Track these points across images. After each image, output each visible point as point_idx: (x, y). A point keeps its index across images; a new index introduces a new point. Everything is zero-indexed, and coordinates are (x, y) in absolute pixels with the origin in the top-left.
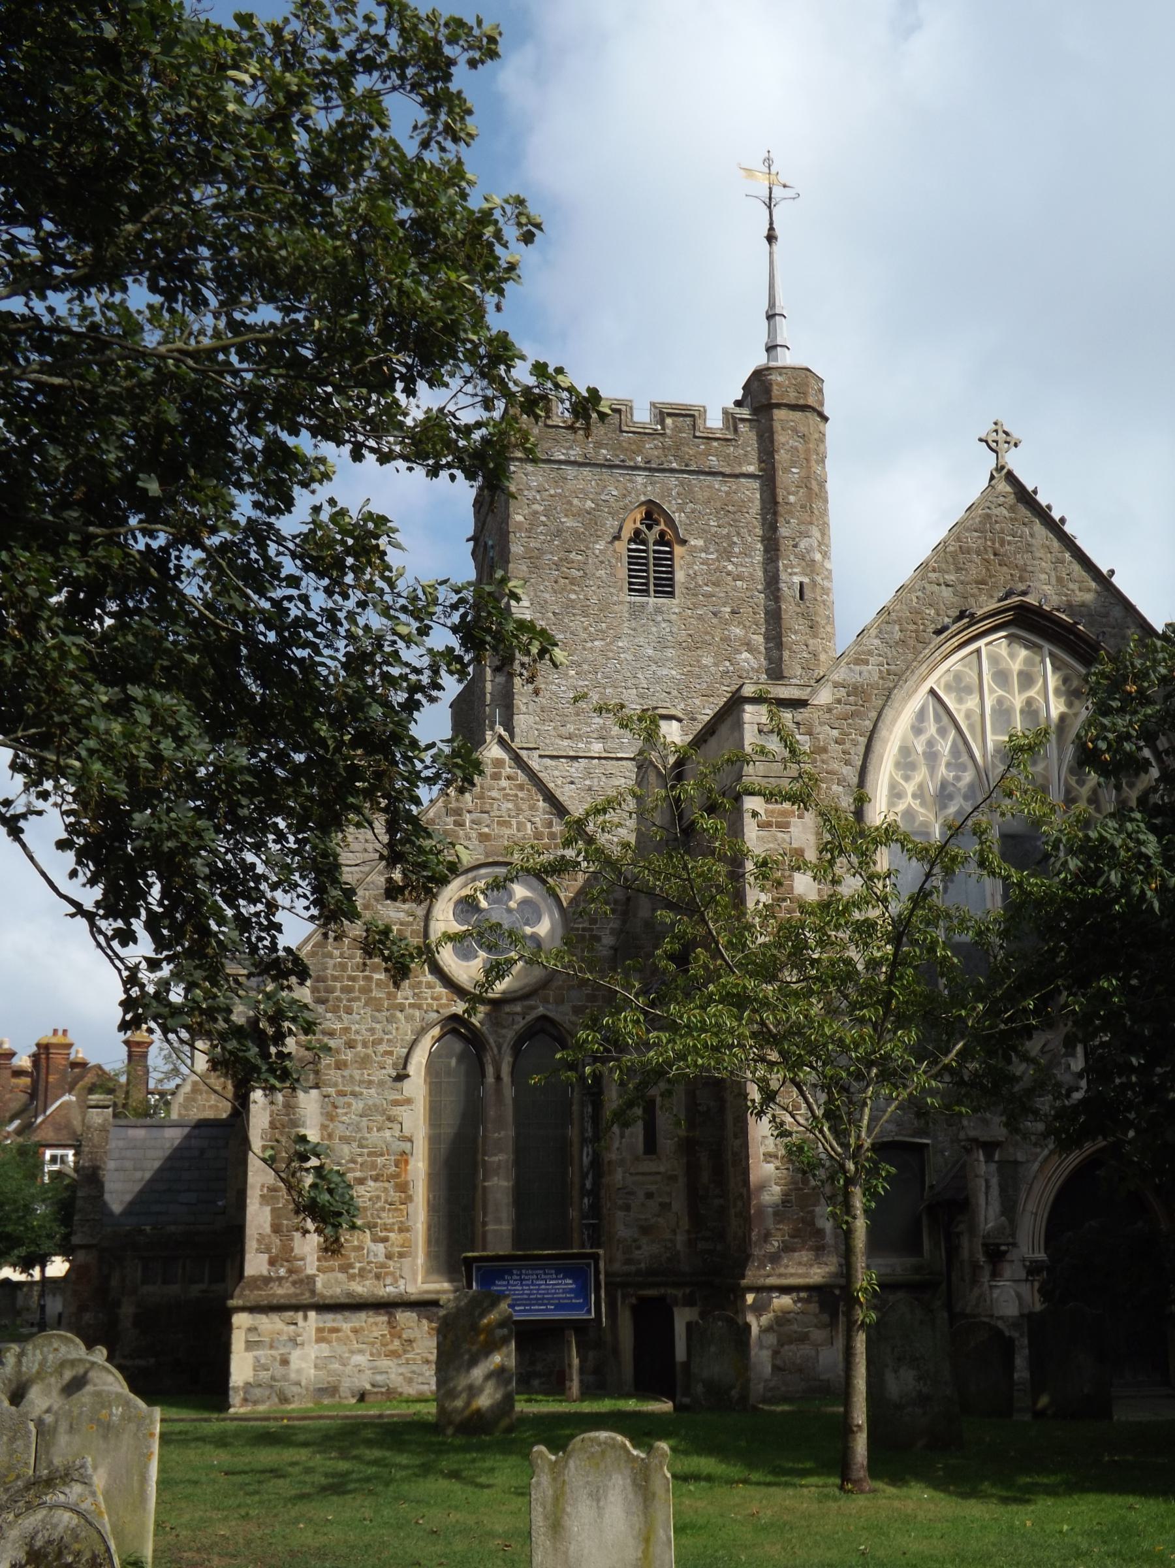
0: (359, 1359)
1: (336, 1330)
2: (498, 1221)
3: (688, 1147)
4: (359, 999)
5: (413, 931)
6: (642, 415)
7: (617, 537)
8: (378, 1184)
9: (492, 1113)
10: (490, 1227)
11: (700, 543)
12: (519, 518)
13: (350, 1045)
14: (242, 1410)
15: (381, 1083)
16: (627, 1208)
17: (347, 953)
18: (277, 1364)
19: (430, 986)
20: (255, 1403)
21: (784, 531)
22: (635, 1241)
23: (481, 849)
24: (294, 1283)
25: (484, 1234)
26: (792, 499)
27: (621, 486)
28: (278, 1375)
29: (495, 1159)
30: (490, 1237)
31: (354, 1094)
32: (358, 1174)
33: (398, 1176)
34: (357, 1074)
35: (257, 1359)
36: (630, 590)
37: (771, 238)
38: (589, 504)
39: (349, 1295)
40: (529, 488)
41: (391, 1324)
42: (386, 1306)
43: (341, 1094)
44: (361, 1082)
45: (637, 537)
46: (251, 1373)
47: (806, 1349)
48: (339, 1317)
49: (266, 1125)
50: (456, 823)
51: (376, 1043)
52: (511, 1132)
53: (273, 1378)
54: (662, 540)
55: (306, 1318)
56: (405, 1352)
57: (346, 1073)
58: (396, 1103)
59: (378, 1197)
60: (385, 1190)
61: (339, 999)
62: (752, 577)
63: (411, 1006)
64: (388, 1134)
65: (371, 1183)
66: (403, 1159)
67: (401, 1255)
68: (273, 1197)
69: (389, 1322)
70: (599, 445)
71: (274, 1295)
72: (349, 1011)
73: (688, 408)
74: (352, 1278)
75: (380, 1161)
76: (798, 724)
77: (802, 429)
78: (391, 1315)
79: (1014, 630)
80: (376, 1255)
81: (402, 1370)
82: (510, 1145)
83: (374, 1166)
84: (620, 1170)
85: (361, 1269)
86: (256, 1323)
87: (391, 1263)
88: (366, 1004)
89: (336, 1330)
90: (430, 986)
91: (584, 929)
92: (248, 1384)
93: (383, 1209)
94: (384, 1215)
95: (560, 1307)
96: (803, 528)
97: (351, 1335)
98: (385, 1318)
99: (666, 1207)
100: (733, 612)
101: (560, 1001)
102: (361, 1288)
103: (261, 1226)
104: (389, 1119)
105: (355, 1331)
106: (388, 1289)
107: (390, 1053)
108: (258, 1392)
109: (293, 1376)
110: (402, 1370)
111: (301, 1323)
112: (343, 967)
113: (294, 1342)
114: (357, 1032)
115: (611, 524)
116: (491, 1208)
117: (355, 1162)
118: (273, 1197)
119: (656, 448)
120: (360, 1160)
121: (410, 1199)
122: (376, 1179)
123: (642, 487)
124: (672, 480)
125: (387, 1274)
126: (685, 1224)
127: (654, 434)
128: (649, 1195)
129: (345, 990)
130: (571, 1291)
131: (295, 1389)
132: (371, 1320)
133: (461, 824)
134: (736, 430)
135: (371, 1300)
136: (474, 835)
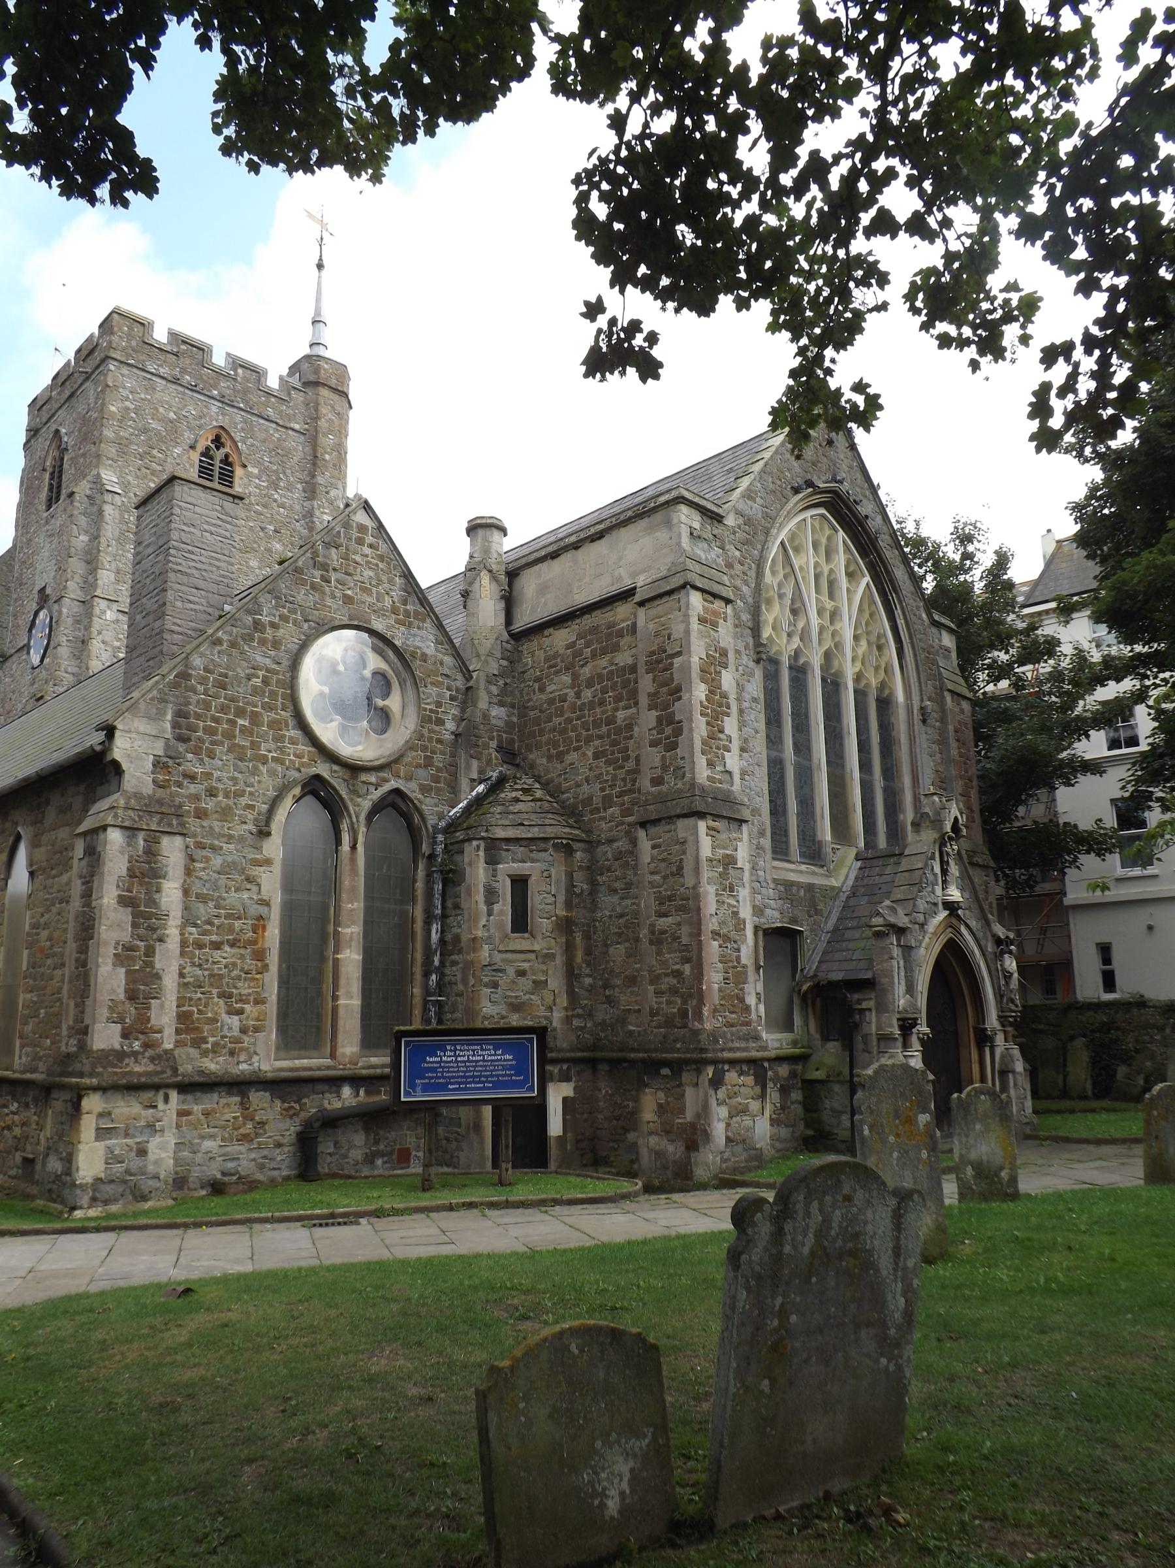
0: (208, 1144)
2: (349, 996)
3: (565, 926)
4: (222, 744)
5: (278, 681)
6: (219, 359)
8: (233, 951)
9: (346, 882)
10: (341, 1002)
11: (256, 471)
12: (113, 409)
13: (212, 793)
14: (92, 1213)
15: (241, 839)
16: (495, 985)
17: (212, 691)
18: (133, 1154)
19: (293, 742)
20: (106, 1202)
21: (320, 479)
25: (335, 1010)
26: (327, 457)
28: (134, 1169)
29: (348, 930)
31: (213, 848)
32: (214, 938)
33: (255, 942)
34: (216, 824)
35: (110, 1149)
37: (320, 266)
38: (172, 415)
39: (201, 1073)
40: (124, 388)
41: (244, 1106)
42: (239, 1086)
43: (202, 846)
45: (206, 453)
49: (124, 873)
53: (128, 1172)
54: (226, 460)
55: (166, 1099)
56: (257, 1135)
57: (205, 823)
59: (234, 965)
60: (242, 957)
64: (246, 895)
65: (227, 948)
66: (260, 924)
67: (257, 1029)
68: (129, 958)
69: (242, 1103)
70: (184, 371)
71: (131, 1073)
72: (211, 756)
73: (255, 366)
74: (205, 1053)
75: (237, 924)
78: (244, 1095)
79: (822, 511)
80: (230, 1029)
81: (253, 1155)
82: (361, 917)
83: (231, 929)
84: (486, 947)
85: (215, 1044)
86: (109, 1106)
87: (246, 1038)
88: (229, 751)
90: (293, 742)
91: (431, 711)
92: (98, 1180)
93: (239, 978)
94: (240, 984)
95: (498, 1085)
98: (238, 1099)
100: (276, 531)
101: (409, 778)
102: (212, 1065)
103: (114, 991)
104: (249, 880)
105: (206, 1114)
107: (252, 807)
108: (109, 1189)
109: (151, 1168)
110: (253, 1155)
111: (161, 1106)
112: (207, 706)
115: (188, 436)
118: (129, 958)
121: (266, 967)
122: (232, 945)
125: (241, 1049)
126: (563, 1001)
128: (521, 973)
130: (511, 1068)
131: (153, 1183)
132: (223, 1101)
135: (227, 1078)
136: (338, 594)
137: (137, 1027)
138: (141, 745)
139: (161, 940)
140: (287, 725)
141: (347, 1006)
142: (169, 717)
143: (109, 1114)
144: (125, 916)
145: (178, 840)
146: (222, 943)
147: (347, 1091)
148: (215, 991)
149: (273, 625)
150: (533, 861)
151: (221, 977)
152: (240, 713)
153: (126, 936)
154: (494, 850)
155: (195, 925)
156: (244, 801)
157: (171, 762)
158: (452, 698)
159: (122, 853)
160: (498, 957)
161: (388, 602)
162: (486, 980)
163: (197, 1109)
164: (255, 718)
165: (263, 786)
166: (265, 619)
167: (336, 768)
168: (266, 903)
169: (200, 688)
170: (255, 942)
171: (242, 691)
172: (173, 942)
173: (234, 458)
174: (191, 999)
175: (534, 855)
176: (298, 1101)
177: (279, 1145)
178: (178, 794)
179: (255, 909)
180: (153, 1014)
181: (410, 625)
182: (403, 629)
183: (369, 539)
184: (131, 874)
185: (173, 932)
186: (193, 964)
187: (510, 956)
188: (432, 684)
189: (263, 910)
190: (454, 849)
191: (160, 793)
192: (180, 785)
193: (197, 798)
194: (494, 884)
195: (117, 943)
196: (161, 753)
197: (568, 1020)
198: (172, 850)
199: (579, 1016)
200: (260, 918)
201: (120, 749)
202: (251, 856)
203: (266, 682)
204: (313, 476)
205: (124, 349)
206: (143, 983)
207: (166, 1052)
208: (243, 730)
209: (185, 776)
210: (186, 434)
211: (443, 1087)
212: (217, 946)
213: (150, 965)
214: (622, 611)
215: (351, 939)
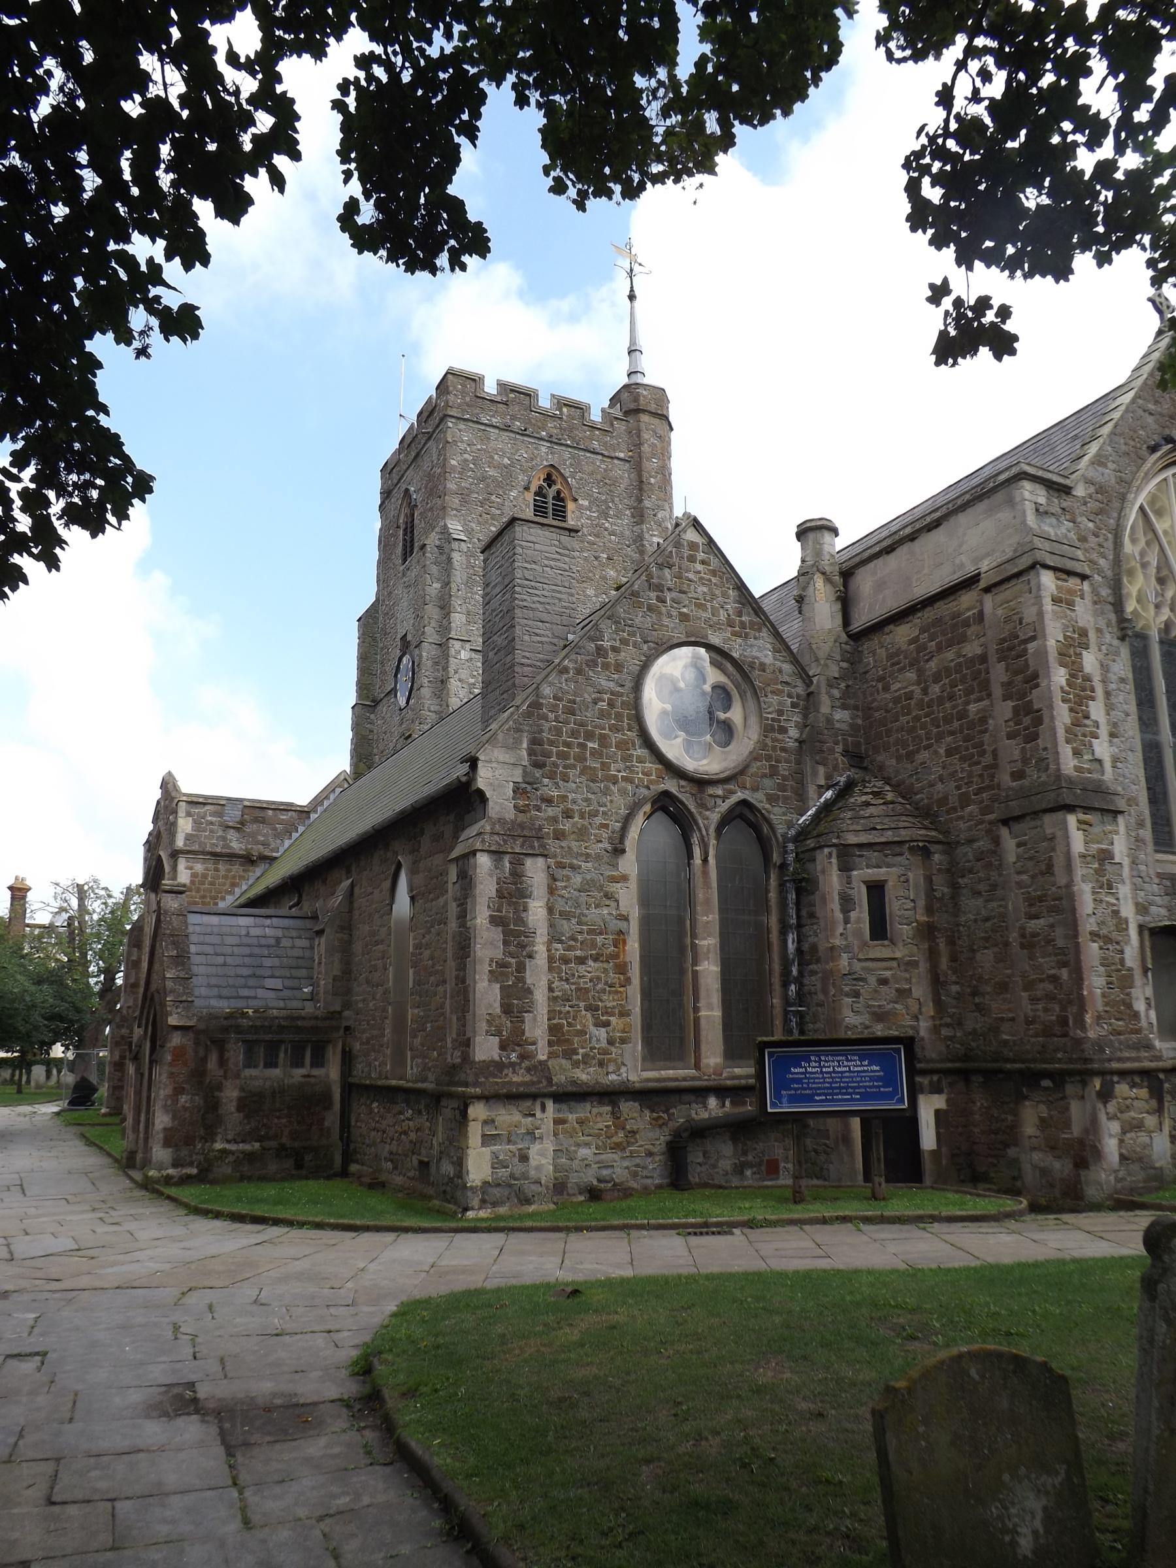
0: (583, 1152)
2: (710, 1007)
3: (927, 932)
4: (574, 767)
5: (623, 703)
8: (597, 965)
9: (700, 895)
10: (702, 1013)
11: (586, 503)
12: (453, 462)
13: (568, 815)
14: (482, 1214)
15: (598, 857)
16: (857, 994)
19: (641, 760)
20: (495, 1204)
21: (647, 503)
23: (682, 628)
24: (528, 1070)
25: (697, 1021)
26: (652, 480)
29: (705, 943)
30: (703, 1022)
31: (573, 868)
32: (578, 953)
33: (617, 956)
35: (495, 1155)
37: (632, 297)
38: (506, 461)
39: (574, 1082)
41: (615, 1115)
42: (610, 1096)
43: (561, 866)
45: (540, 492)
46: (490, 1171)
47: (1143, 1138)
49: (494, 894)
51: (594, 814)
53: (512, 1176)
54: (558, 497)
55: (543, 1109)
56: (629, 1144)
58: (614, 880)
59: (599, 978)
61: (555, 765)
62: (622, 535)
65: (591, 963)
66: (620, 938)
67: (623, 1041)
69: (613, 1113)
70: (514, 418)
71: (510, 1083)
73: (579, 403)
74: (576, 1064)
76: (1063, 509)
77: (660, 432)
78: (614, 1104)
80: (598, 1040)
81: (626, 1163)
83: (594, 945)
85: (585, 1056)
86: (493, 1114)
87: (613, 1050)
88: (582, 773)
90: (641, 760)
91: (773, 720)
93: (604, 991)
95: (866, 1096)
96: (660, 503)
98: (609, 1108)
99: (903, 994)
100: (609, 558)
101: (755, 789)
102: (583, 1076)
103: (491, 1006)
104: (607, 896)
105: (581, 1122)
106: (612, 1077)
107: (606, 826)
108: (496, 1192)
110: (626, 1163)
111: (539, 1114)
112: (558, 731)
113: (531, 1135)
115: (522, 478)
118: (502, 974)
119: (555, 427)
121: (628, 981)
122: (596, 960)
123: (545, 455)
124: (567, 454)
125: (610, 1060)
126: (929, 1010)
127: (554, 416)
128: (884, 982)
129: (561, 755)
130: (879, 1079)
131: (535, 1188)
132: (595, 1110)
134: (612, 425)
135: (598, 1088)
137: (514, 1040)
138: (501, 773)
139: (530, 956)
141: (707, 1017)
142: (525, 745)
144: (497, 934)
145: (540, 861)
146: (586, 958)
147: (712, 1102)
148: (582, 1004)
149: (615, 649)
151: (587, 990)
152: (590, 736)
153: (498, 953)
154: (847, 857)
156: (598, 820)
158: (794, 705)
159: (491, 876)
160: (858, 966)
161: (723, 615)
163: (572, 1117)
166: (607, 644)
168: (626, 919)
169: (551, 716)
170: (617, 956)
171: (589, 715)
172: (541, 959)
173: (565, 493)
174: (560, 1012)
176: (667, 1111)
177: (650, 1154)
178: (537, 818)
179: (615, 925)
181: (746, 636)
182: (739, 640)
183: (701, 556)
184: (500, 894)
185: (540, 948)
186: (561, 979)
187: (870, 964)
188: (773, 692)
189: (622, 925)
190: (805, 857)
191: (522, 817)
192: (539, 809)
193: (554, 820)
196: (520, 780)
197: (936, 1029)
198: (536, 871)
199: (947, 1025)
201: (484, 779)
203: (611, 704)
204: (640, 501)
205: (460, 405)
206: (515, 1000)
207: (540, 1062)
208: (594, 752)
211: (809, 1099)
212: (581, 961)
213: (522, 980)
214: (967, 599)
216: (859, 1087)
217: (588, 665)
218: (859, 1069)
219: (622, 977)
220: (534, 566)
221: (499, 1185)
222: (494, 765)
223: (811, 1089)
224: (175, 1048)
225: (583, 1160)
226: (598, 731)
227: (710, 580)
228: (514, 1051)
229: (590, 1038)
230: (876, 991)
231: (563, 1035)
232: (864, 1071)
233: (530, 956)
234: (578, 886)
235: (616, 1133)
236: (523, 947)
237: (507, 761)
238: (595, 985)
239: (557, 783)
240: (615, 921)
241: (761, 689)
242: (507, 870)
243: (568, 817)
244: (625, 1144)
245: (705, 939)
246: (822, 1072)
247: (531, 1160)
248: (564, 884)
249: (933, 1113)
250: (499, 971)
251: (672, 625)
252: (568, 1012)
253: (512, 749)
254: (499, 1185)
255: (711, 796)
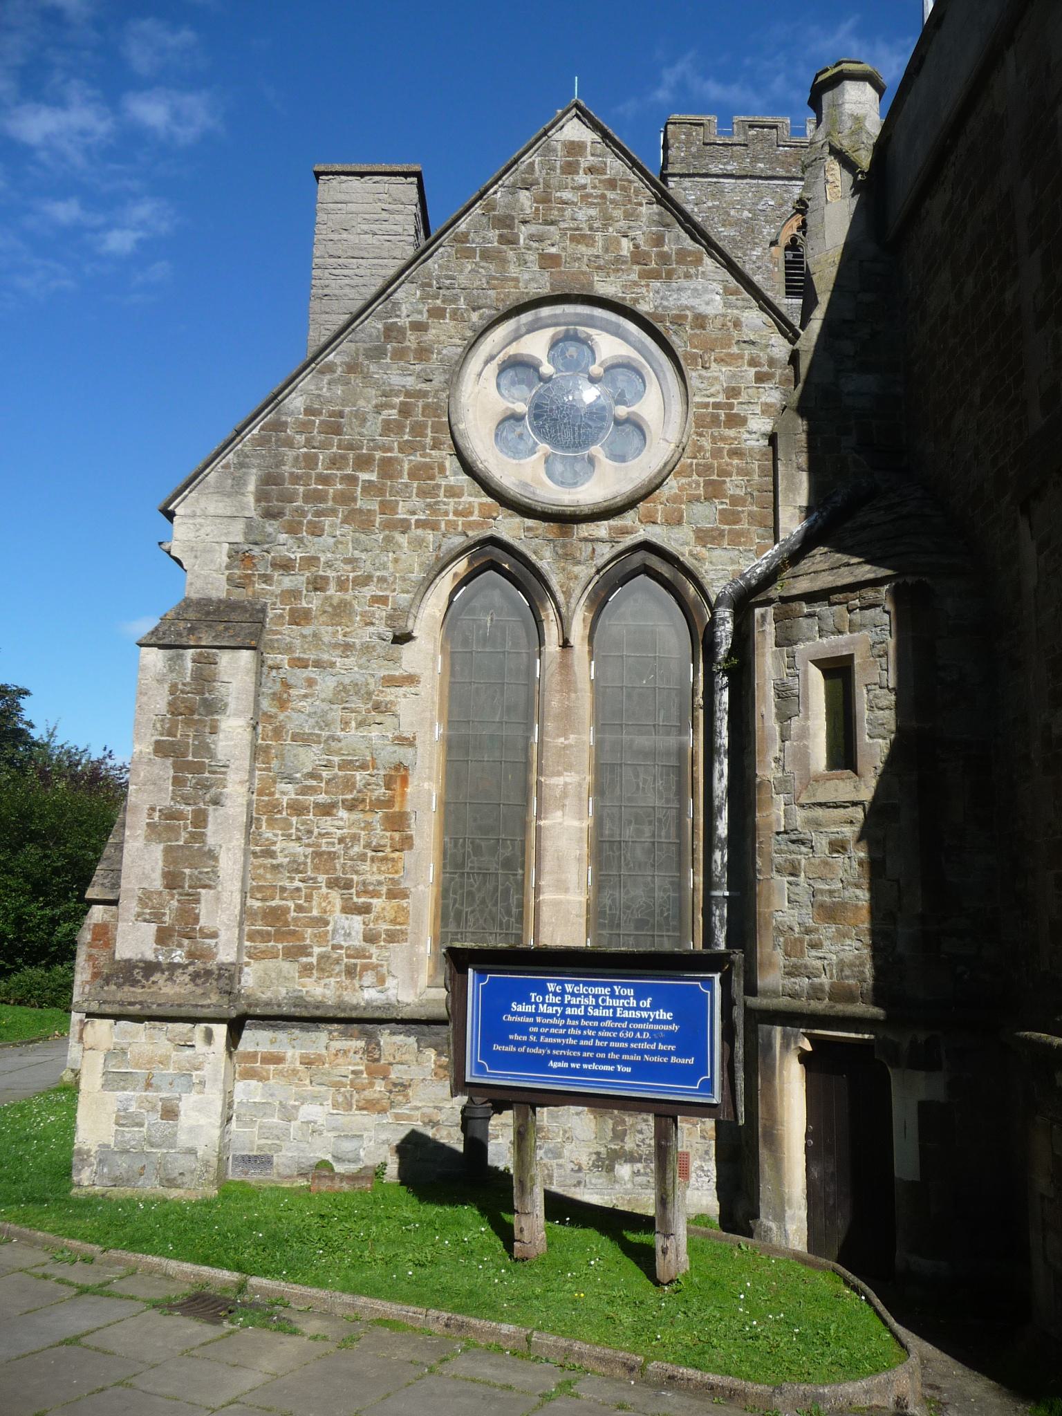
0: (313, 1112)
1: (278, 1059)
2: (562, 887)
4: (333, 512)
7: (773, 243)
9: (554, 703)
13: (318, 585)
15: (367, 649)
22: (808, 931)
27: (778, 196)
29: (559, 781)
32: (322, 798)
33: (389, 803)
34: (326, 633)
36: (787, 293)
38: (746, 214)
39: (299, 1001)
41: (372, 1053)
42: (363, 1023)
44: (336, 646)
48: (282, 1036)
50: (503, 239)
51: (365, 580)
52: (589, 737)
55: (209, 1037)
56: (392, 1104)
57: (307, 630)
58: (391, 682)
59: (355, 838)
61: (301, 512)
63: (420, 524)
64: (375, 732)
65: (343, 813)
66: (399, 775)
67: (392, 937)
68: (169, 828)
69: (367, 1051)
70: (755, 159)
74: (307, 970)
75: (359, 776)
78: (371, 1038)
82: (585, 759)
83: (349, 784)
84: (780, 799)
85: (322, 957)
86: (123, 1042)
87: (373, 949)
89: (278, 1059)
90: (453, 492)
91: (717, 406)
93: (362, 857)
95: (643, 1070)
97: (301, 1068)
98: (361, 1044)
101: (675, 520)
102: (322, 991)
103: (146, 877)
107: (383, 600)
112: (311, 461)
114: (329, 565)
115: (768, 232)
116: (548, 864)
117: (317, 777)
120: (325, 774)
121: (406, 843)
122: (351, 807)
130: (668, 1038)
133: (511, 241)
136: (532, 257)
137: (181, 927)
138: (211, 531)
139: (216, 802)
140: (442, 469)
141: (557, 904)
142: (251, 487)
143: (124, 1052)
144: (165, 769)
146: (333, 805)
148: (322, 878)
149: (419, 327)
150: (853, 628)
151: (332, 856)
152: (364, 463)
155: (290, 780)
157: (256, 551)
158: (760, 378)
159: (160, 682)
160: (800, 815)
161: (626, 246)
162: (778, 859)
164: (388, 468)
165: (401, 566)
166: (403, 321)
167: (530, 522)
169: (301, 439)
170: (389, 803)
174: (283, 889)
175: (857, 616)
178: (265, 593)
179: (389, 754)
180: (203, 909)
181: (670, 275)
182: (656, 284)
184: (174, 709)
186: (288, 837)
187: (819, 812)
188: (719, 361)
189: (404, 754)
191: (239, 595)
192: (266, 579)
193: (294, 594)
194: (793, 683)
195: (153, 809)
196: (240, 539)
200: (399, 766)
202: (383, 673)
203: (405, 410)
205: (683, 159)
208: (369, 487)
209: (274, 565)
210: (765, 231)
211: (538, 1064)
212: (326, 810)
213: (199, 837)
215: (565, 795)
216: (629, 1051)
217: (368, 357)
218: (632, 1014)
219: (397, 835)
220: (345, 235)
221: (125, 1152)
222: (199, 520)
223: (543, 1046)
224: (96, 925)
225: (309, 1122)
226: (378, 455)
227: (603, 197)
228: (180, 946)
229: (335, 931)
230: (826, 863)
231: (286, 924)
232: (641, 1020)
233: (216, 802)
234: (329, 694)
235: (372, 1084)
236: (204, 786)
237: (220, 512)
238: (347, 848)
239: (301, 540)
240: (391, 749)
241: (693, 358)
242: (189, 672)
243: (316, 589)
244: (385, 1102)
245: (559, 774)
246: (564, 1016)
247: (182, 1118)
248: (303, 691)
249: (914, 1108)
250: (164, 824)
251: (527, 276)
252: (298, 889)
253: (229, 495)
254: (125, 1152)
255: (586, 540)
